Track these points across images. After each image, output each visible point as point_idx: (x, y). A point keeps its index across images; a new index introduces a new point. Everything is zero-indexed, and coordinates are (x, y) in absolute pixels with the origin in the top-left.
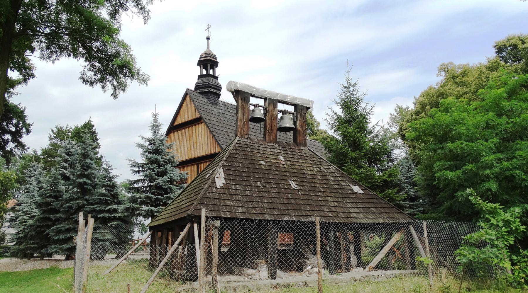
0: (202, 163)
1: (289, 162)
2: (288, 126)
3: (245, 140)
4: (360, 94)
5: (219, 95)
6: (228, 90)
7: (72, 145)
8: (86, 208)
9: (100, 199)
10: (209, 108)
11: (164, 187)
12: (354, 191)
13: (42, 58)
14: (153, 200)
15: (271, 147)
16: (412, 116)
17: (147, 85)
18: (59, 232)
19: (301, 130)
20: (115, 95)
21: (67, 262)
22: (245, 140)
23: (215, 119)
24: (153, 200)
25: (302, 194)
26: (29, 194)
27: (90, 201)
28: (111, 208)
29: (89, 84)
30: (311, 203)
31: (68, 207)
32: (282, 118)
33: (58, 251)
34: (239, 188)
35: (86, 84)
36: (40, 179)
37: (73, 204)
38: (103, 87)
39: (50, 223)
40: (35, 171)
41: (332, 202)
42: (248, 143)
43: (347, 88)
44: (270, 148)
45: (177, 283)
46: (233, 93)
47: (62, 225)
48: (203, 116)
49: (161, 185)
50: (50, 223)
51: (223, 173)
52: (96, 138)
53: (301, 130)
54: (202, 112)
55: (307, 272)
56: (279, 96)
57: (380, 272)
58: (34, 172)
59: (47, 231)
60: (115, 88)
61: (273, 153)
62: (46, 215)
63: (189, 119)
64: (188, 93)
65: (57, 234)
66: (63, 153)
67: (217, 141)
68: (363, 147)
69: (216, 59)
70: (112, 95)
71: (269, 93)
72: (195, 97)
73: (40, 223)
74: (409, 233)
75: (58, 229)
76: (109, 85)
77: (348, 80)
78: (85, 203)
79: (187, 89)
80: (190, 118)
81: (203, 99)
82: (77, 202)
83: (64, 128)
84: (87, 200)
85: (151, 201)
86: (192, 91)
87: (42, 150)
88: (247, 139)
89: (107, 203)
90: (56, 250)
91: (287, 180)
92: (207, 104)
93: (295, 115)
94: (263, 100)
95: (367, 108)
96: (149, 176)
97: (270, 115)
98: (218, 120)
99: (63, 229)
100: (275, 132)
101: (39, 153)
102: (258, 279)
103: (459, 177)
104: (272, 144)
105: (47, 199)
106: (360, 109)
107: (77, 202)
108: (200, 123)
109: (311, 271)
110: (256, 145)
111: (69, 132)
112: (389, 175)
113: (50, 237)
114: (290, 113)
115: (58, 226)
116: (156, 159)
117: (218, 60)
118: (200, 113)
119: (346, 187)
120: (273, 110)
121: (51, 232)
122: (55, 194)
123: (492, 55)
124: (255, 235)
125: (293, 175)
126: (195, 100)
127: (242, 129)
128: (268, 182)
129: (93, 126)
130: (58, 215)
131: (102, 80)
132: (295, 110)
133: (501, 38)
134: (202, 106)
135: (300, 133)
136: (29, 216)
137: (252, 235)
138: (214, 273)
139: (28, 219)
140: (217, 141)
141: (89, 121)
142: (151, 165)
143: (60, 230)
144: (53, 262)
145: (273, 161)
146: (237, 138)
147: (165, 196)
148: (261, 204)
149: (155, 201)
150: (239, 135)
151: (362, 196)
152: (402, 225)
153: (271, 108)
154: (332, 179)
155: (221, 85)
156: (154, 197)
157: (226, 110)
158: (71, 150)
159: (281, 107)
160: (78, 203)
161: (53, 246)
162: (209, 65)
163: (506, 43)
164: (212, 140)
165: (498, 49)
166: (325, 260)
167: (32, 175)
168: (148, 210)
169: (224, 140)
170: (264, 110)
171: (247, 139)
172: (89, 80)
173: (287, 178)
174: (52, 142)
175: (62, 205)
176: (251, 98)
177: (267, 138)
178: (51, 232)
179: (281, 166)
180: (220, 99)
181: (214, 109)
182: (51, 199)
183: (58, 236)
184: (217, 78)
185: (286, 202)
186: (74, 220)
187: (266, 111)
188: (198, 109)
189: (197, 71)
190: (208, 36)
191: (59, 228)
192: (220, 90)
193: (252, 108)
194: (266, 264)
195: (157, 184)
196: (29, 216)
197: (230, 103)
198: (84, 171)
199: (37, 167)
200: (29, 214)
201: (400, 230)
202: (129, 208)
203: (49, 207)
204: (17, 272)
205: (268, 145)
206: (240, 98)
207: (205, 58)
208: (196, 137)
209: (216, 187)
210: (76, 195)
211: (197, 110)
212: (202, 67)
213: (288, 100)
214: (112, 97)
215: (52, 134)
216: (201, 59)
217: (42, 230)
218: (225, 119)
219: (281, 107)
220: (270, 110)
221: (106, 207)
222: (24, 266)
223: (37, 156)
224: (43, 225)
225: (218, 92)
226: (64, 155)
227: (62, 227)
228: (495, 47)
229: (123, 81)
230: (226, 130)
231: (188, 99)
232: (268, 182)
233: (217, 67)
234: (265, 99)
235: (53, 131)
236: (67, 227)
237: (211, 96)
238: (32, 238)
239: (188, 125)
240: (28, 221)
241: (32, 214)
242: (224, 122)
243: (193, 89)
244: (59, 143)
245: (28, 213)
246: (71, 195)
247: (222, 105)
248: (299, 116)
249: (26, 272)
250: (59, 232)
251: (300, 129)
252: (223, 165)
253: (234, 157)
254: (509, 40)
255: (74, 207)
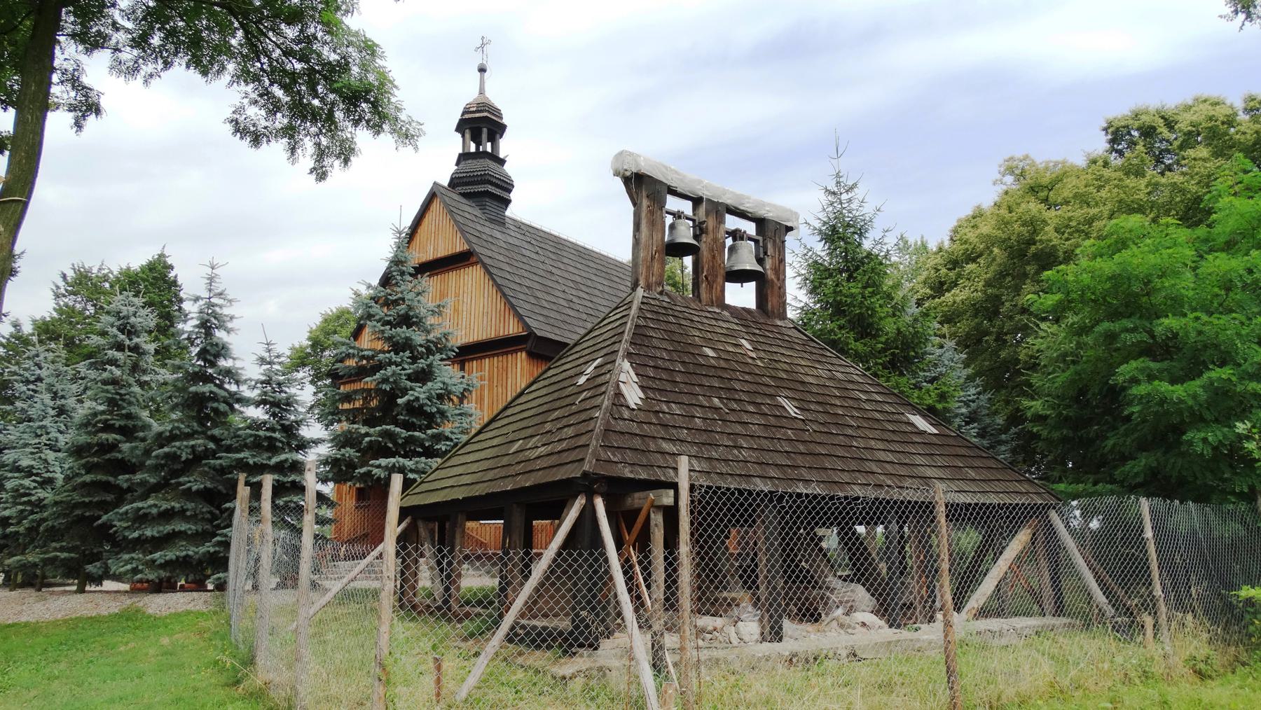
0: (472, 360)
1: (762, 355)
2: (748, 268)
3: (658, 296)
4: (868, 210)
5: (507, 202)
6: (616, 174)
7: (132, 309)
8: (220, 458)
9: (256, 436)
10: (487, 230)
11: (428, 409)
12: (917, 428)
13: (118, 67)
14: (400, 441)
15: (716, 316)
16: (937, 270)
17: (416, 148)
18: (141, 519)
19: (775, 280)
20: (320, 174)
21: (79, 595)
22: (658, 296)
23: (501, 258)
24: (400, 441)
25: (815, 431)
26: (31, 424)
27: (224, 442)
28: (286, 460)
29: (249, 139)
30: (840, 452)
31: (167, 455)
32: (732, 249)
33: (140, 567)
34: (676, 409)
35: (242, 138)
36: (58, 387)
37: (179, 448)
38: (293, 150)
39: (110, 498)
40: (40, 368)
41: (882, 452)
42: (665, 304)
43: (834, 193)
44: (716, 319)
45: (549, 654)
46: (627, 181)
47: (150, 502)
48: (478, 249)
49: (422, 406)
50: (110, 498)
51: (632, 373)
52: (176, 295)
53: (775, 280)
54: (474, 240)
55: (834, 624)
56: (727, 196)
57: (994, 624)
58: (38, 372)
59: (105, 518)
60: (321, 154)
61: (724, 331)
62: (99, 477)
63: (439, 256)
64: (438, 194)
65: (137, 525)
66: (112, 326)
67: (513, 307)
68: (878, 330)
69: (502, 118)
70: (311, 172)
71: (705, 187)
72: (454, 204)
73: (83, 496)
74: (1050, 531)
75: (141, 512)
76: (308, 144)
77: (838, 175)
78: (211, 445)
79: (435, 183)
80: (442, 252)
81: (470, 210)
82: (192, 443)
83: (95, 270)
84: (213, 439)
85: (395, 444)
86: (443, 187)
87: (34, 321)
88: (661, 293)
89: (272, 448)
90: (134, 565)
91: (772, 396)
92: (482, 222)
93: (761, 244)
94: (689, 204)
95: (886, 240)
96: (391, 380)
97: (709, 240)
98: (508, 260)
99: (154, 511)
100: (720, 280)
101: (27, 329)
102: (735, 641)
103: (1195, 397)
104: (718, 311)
105: (104, 436)
106: (867, 245)
107: (192, 443)
108: (468, 266)
109: (847, 620)
110: (684, 309)
111: (106, 281)
112: (938, 395)
113: (116, 532)
114: (750, 239)
115: (140, 505)
116: (408, 339)
117: (505, 121)
118: (468, 242)
119: (896, 416)
120: (716, 229)
121: (117, 519)
122: (122, 423)
123: (1099, 144)
124: (805, 529)
125: (781, 384)
126: (455, 210)
127: (649, 268)
128: (734, 400)
129: (171, 267)
130: (138, 477)
131: (289, 132)
132: (759, 231)
133: (1120, 110)
134: (471, 224)
135: (773, 287)
136: (38, 479)
137: (799, 529)
138: (656, 627)
139: (35, 488)
140: (513, 307)
141: (161, 256)
142: (397, 353)
143: (146, 515)
144: (123, 597)
145: (731, 349)
146: (640, 292)
147: (429, 432)
148: (736, 452)
149: (403, 445)
150: (642, 283)
151: (935, 440)
152: (1020, 509)
153: (711, 223)
154: (863, 397)
155: (513, 178)
156: (404, 433)
157: (522, 237)
158: (132, 320)
159: (732, 222)
160: (193, 447)
161: (126, 557)
162: (485, 130)
163: (1131, 122)
164: (500, 305)
165: (1113, 133)
166: (876, 590)
167: (32, 378)
168: (394, 464)
169: (528, 306)
170: (694, 227)
171: (661, 293)
172: (252, 129)
173: (772, 391)
174: (62, 303)
175: (147, 453)
176: (670, 199)
177: (704, 295)
178: (117, 519)
179: (750, 361)
180: (511, 212)
181: (498, 235)
182: (114, 436)
183: (138, 528)
184: (502, 162)
185: (787, 449)
186: (184, 490)
187: (701, 229)
188: (462, 232)
189: (455, 144)
190: (482, 64)
191: (143, 508)
192: (509, 191)
193: (669, 220)
194: (755, 605)
195: (413, 401)
196: (38, 479)
197: (528, 223)
198: (205, 366)
199: (45, 358)
200: (37, 475)
201: (1027, 522)
202: (339, 459)
203: (108, 456)
204: (26, 624)
205: (709, 312)
206: (644, 194)
207: (477, 115)
208: (457, 295)
209: (628, 407)
210: (189, 426)
211: (462, 234)
212: (468, 136)
213: (746, 206)
214: (314, 176)
215: (61, 283)
216: (467, 116)
217: (87, 514)
218: (525, 260)
219: (732, 222)
220: (710, 228)
221: (270, 458)
222: (39, 607)
223: (21, 337)
224: (91, 502)
225: (504, 194)
226: (115, 330)
227: (150, 507)
228: (1106, 129)
229: (347, 139)
230: (528, 283)
231: (436, 206)
232: (734, 400)
233: (501, 137)
234: (697, 201)
235: (64, 277)
236: (165, 506)
237: (489, 203)
238: (53, 534)
239: (461, 262)
240: (34, 492)
241: (46, 475)
242: (521, 265)
243: (445, 182)
244: (78, 306)
245: (35, 471)
246: (176, 424)
247: (512, 227)
248: (769, 246)
249: (55, 624)
250: (141, 519)
251: (773, 277)
252: (629, 355)
253: (646, 336)
254: (1136, 116)
255: (184, 457)
